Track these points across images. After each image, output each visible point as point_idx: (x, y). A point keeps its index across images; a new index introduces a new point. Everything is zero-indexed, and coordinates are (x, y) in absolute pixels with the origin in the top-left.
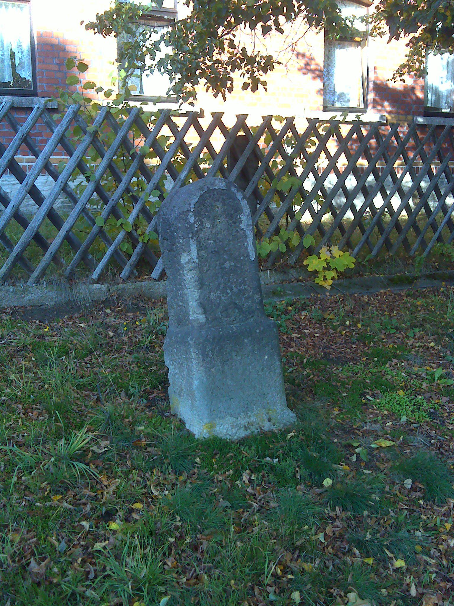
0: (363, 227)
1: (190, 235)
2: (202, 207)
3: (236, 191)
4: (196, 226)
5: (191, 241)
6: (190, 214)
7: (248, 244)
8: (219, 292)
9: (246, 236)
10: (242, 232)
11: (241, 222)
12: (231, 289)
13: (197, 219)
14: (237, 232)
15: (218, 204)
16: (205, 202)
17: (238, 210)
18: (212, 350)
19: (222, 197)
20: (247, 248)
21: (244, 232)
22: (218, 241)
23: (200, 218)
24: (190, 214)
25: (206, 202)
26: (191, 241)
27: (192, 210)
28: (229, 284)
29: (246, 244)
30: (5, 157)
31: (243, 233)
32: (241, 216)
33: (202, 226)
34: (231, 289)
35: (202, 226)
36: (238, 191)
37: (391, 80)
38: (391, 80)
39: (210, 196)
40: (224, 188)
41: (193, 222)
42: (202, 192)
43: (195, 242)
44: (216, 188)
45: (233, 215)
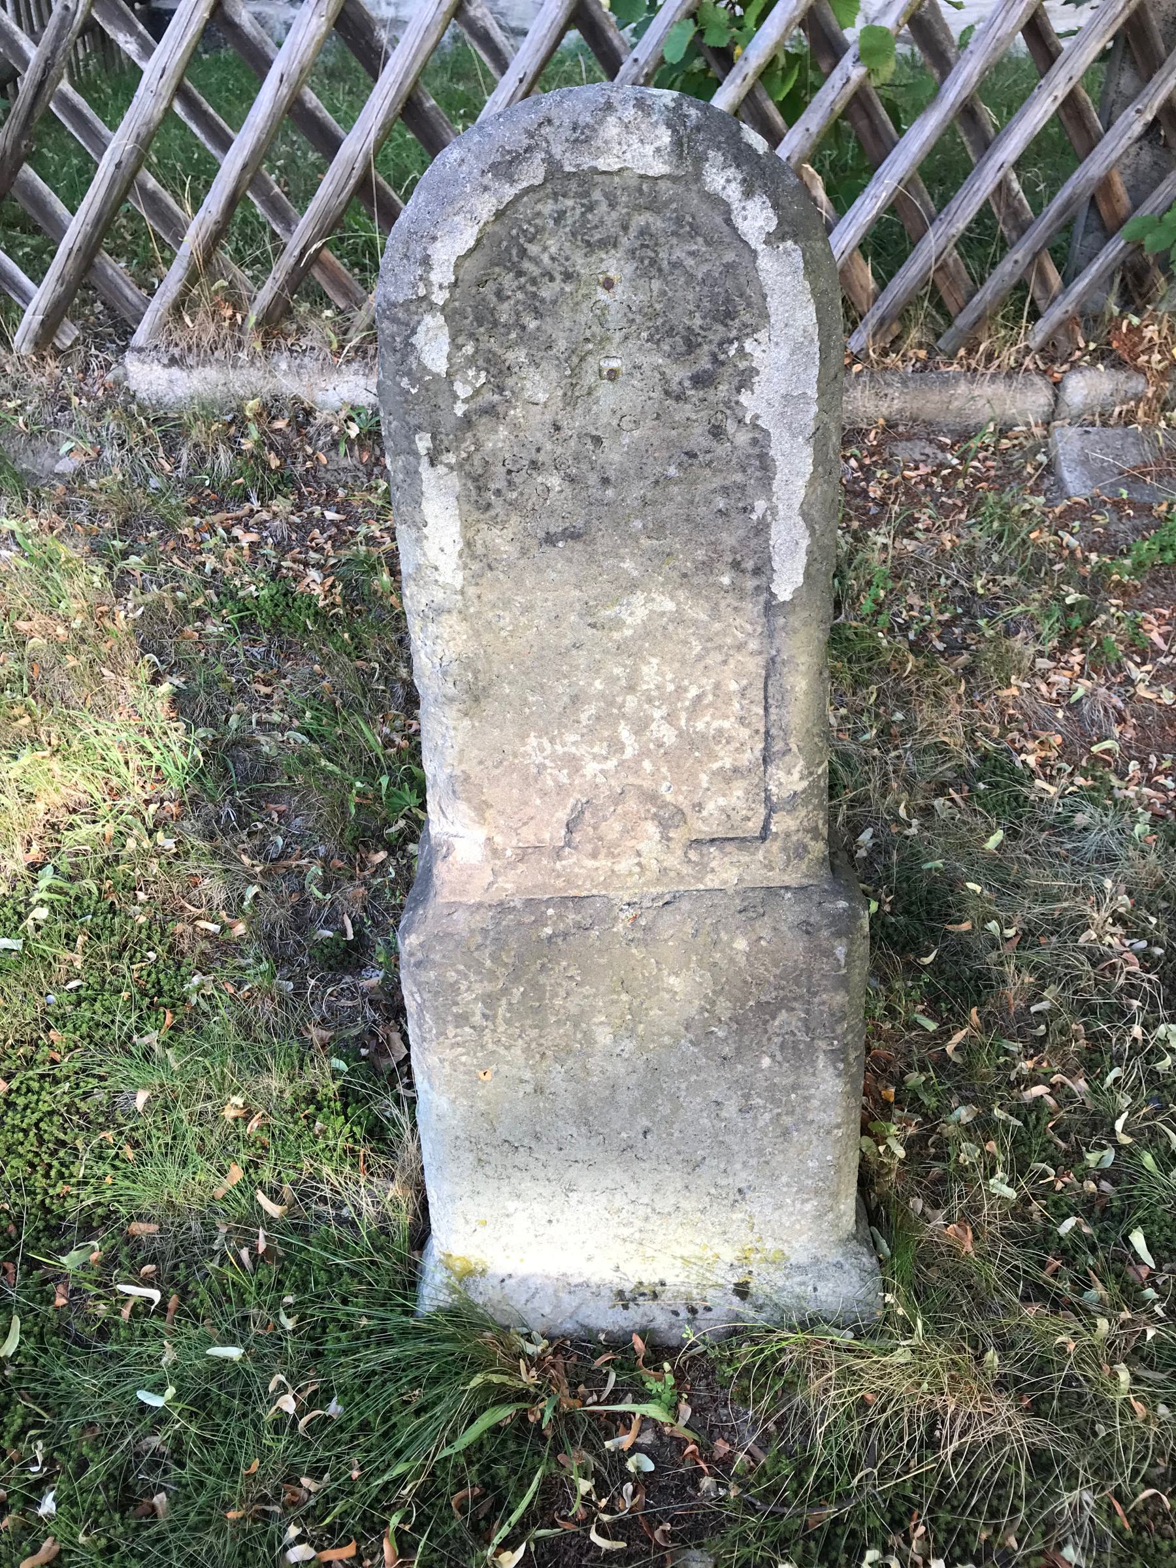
0: (312, 139)
1: (423, 443)
2: (508, 281)
3: (733, 193)
4: (463, 390)
5: (426, 472)
6: (428, 318)
7: (773, 510)
8: (570, 738)
9: (765, 465)
10: (742, 438)
11: (745, 380)
12: (641, 726)
13: (469, 349)
14: (717, 432)
15: (614, 265)
16: (523, 253)
17: (733, 306)
18: (490, 1000)
19: (640, 220)
20: (761, 529)
21: (761, 439)
22: (593, 479)
23: (493, 344)
24: (428, 318)
25: (533, 249)
26: (426, 472)
27: (440, 297)
28: (631, 702)
29: (760, 505)
30: (241, 149)
31: (755, 442)
32: (749, 345)
33: (501, 389)
34: (641, 726)
35: (501, 389)
36: (748, 194)
37: (639, 864)
38: (639, 864)
39: (559, 217)
40: (659, 168)
41: (439, 365)
42: (509, 192)
43: (454, 481)
44: (601, 164)
45: (707, 331)
